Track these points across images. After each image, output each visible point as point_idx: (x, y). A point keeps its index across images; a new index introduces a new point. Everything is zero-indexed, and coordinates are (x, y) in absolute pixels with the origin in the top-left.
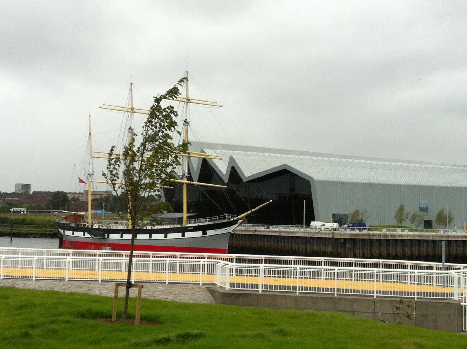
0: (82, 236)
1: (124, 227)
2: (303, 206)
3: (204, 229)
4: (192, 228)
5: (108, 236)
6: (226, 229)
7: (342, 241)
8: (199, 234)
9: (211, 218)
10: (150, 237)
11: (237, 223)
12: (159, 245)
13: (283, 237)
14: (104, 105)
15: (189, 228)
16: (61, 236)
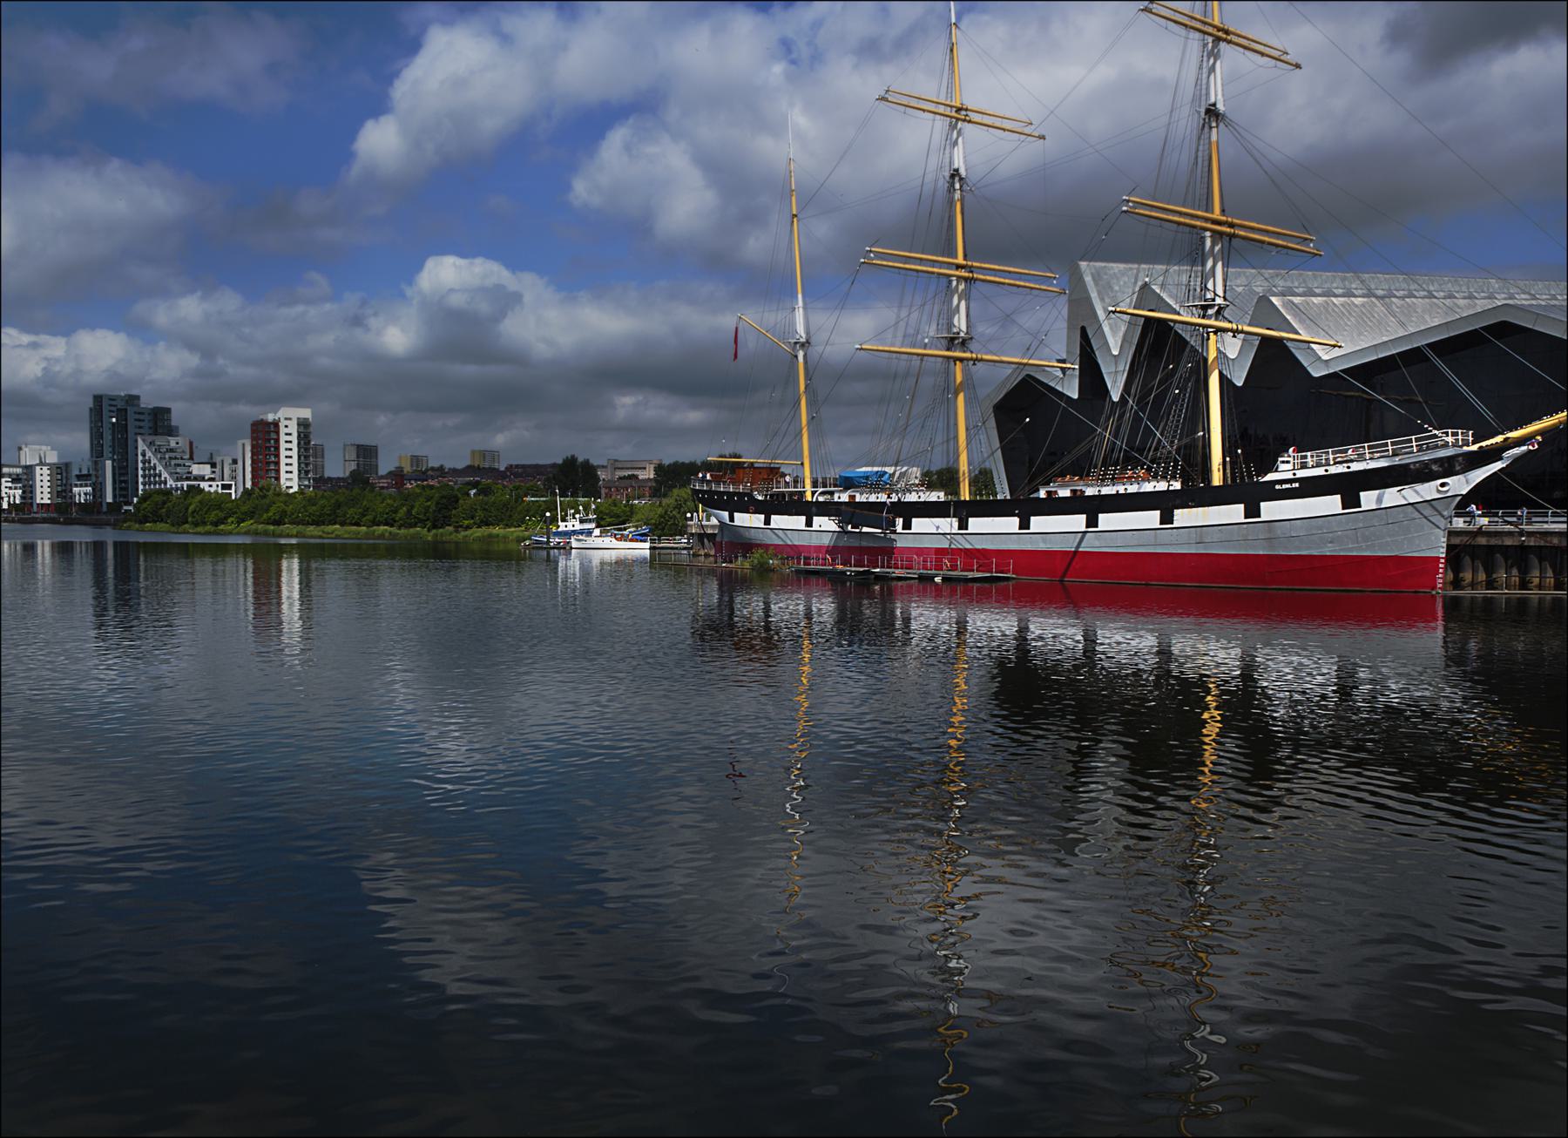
0: (955, 530)
1: (199, 469)
2: (891, 249)
3: (1349, 487)
4: (1297, 485)
5: (907, 525)
6: (1443, 485)
7: (302, 429)
8: (1331, 504)
9: (1347, 450)
10: (767, 522)
11: (1501, 459)
12: (1328, 550)
13: (255, 450)
14: (887, 91)
15: (1278, 487)
16: (440, 525)
